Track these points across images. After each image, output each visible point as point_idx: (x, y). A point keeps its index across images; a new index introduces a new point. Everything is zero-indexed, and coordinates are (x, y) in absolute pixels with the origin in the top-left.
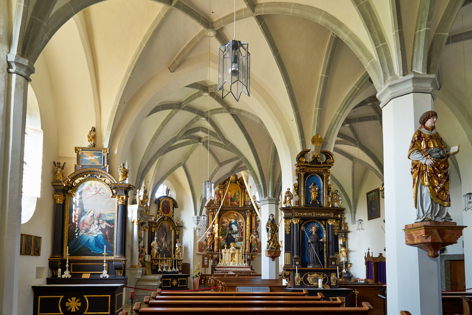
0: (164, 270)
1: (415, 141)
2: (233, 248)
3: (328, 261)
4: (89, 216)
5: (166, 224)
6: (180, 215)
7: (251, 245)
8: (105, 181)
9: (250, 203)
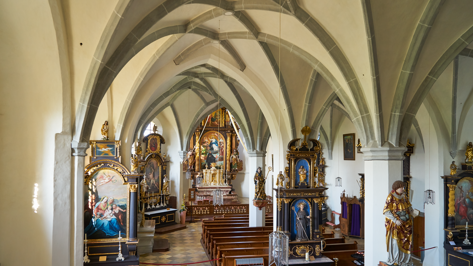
0: (153, 206)
1: (389, 203)
2: (214, 168)
3: (313, 234)
4: (103, 202)
5: (154, 161)
6: (166, 150)
7: (231, 164)
8: (117, 170)
9: (230, 123)
